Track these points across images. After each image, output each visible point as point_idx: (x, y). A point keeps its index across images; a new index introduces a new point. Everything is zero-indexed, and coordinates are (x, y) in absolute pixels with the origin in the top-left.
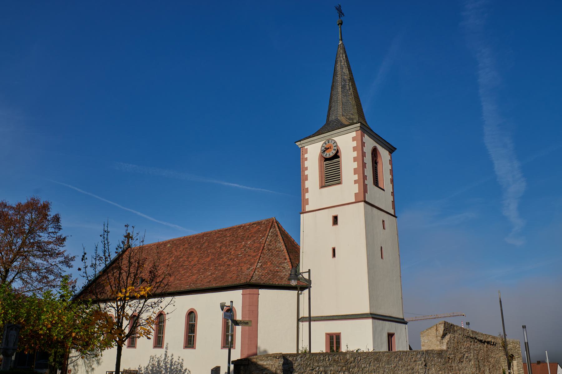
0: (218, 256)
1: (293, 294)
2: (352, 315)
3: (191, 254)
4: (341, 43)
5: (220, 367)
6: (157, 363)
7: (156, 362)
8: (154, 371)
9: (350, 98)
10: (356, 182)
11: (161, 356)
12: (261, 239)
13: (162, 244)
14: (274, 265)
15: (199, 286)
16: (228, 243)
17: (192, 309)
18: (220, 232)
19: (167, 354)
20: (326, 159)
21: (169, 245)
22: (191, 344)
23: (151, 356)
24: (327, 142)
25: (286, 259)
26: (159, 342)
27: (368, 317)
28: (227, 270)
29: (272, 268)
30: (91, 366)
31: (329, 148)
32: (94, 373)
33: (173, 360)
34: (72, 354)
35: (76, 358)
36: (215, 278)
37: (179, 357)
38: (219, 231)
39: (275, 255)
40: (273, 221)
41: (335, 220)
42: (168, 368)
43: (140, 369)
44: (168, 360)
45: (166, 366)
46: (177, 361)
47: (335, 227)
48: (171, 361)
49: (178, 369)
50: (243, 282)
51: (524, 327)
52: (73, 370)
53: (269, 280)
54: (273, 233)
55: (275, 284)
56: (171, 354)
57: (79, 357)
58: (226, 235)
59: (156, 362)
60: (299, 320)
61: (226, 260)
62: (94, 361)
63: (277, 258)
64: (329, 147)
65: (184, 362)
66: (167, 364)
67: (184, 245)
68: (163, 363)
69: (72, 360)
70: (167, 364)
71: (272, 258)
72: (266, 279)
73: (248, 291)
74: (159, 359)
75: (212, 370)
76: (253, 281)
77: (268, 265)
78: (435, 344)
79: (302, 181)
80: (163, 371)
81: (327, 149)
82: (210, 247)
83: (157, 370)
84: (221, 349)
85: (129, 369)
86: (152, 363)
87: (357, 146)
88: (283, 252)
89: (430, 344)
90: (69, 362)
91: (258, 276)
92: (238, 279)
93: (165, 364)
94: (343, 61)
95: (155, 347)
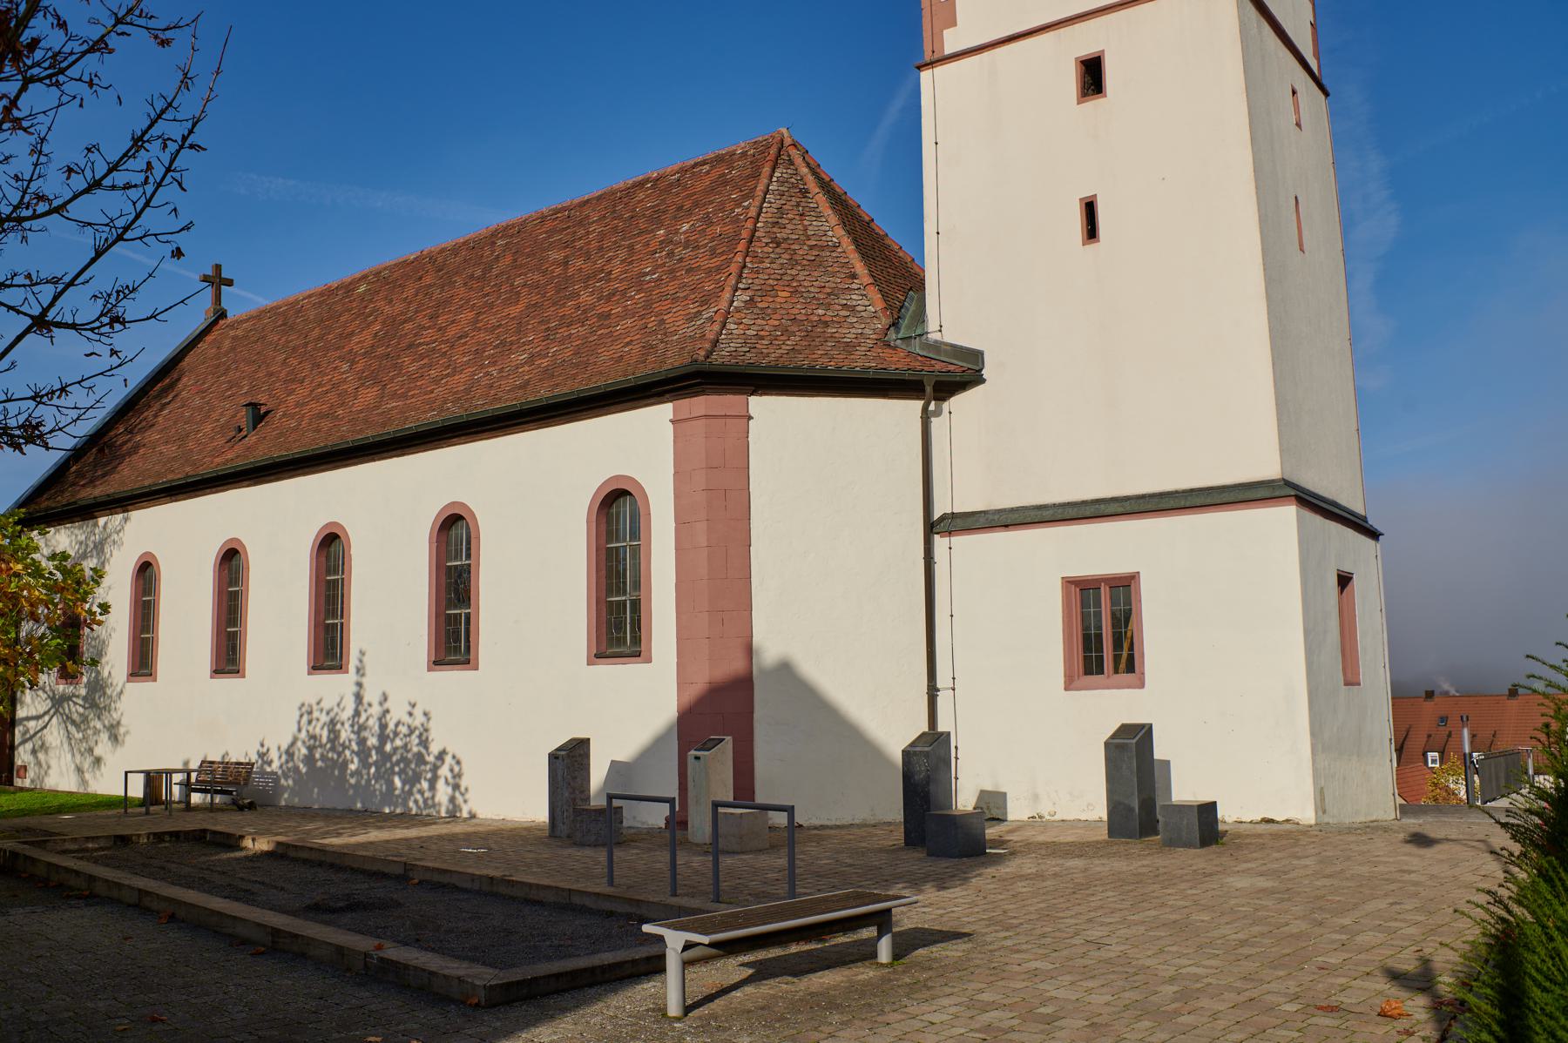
0: (558, 292)
2: (1192, 490)
3: (448, 302)
5: (589, 739)
6: (326, 729)
7: (322, 728)
8: (317, 761)
11: (338, 705)
12: (739, 205)
13: (337, 288)
14: (805, 298)
15: (481, 405)
16: (594, 244)
17: (454, 504)
18: (559, 215)
19: (362, 692)
21: (362, 289)
22: (457, 650)
23: (303, 705)
25: (854, 276)
26: (332, 649)
27: (1277, 494)
28: (600, 332)
29: (798, 310)
30: (91, 750)
32: (102, 775)
33: (388, 717)
34: (25, 709)
35: (41, 723)
36: (546, 370)
37: (414, 706)
38: (557, 211)
39: (805, 262)
40: (782, 141)
41: (1092, 75)
42: (369, 750)
43: (264, 754)
44: (367, 719)
45: (362, 742)
46: (406, 719)
47: (1094, 104)
48: (380, 719)
49: (408, 751)
50: (676, 364)
52: (32, 765)
54: (786, 184)
55: (825, 369)
56: (381, 693)
57: (50, 720)
58: (587, 217)
59: (322, 728)
60: (932, 527)
61: (591, 300)
62: (99, 731)
63: (816, 274)
65: (432, 725)
66: (365, 734)
67: (420, 278)
68: (349, 729)
69: (27, 731)
70: (365, 734)
71: (794, 272)
73: (700, 404)
74: (332, 714)
75: (553, 757)
76: (722, 357)
77: (778, 300)
80: (352, 762)
82: (521, 266)
83: (328, 759)
84: (589, 663)
85: (223, 757)
86: (308, 731)
88: (839, 250)
90: (18, 739)
91: (739, 341)
92: (651, 358)
93: (358, 733)
95: (316, 667)
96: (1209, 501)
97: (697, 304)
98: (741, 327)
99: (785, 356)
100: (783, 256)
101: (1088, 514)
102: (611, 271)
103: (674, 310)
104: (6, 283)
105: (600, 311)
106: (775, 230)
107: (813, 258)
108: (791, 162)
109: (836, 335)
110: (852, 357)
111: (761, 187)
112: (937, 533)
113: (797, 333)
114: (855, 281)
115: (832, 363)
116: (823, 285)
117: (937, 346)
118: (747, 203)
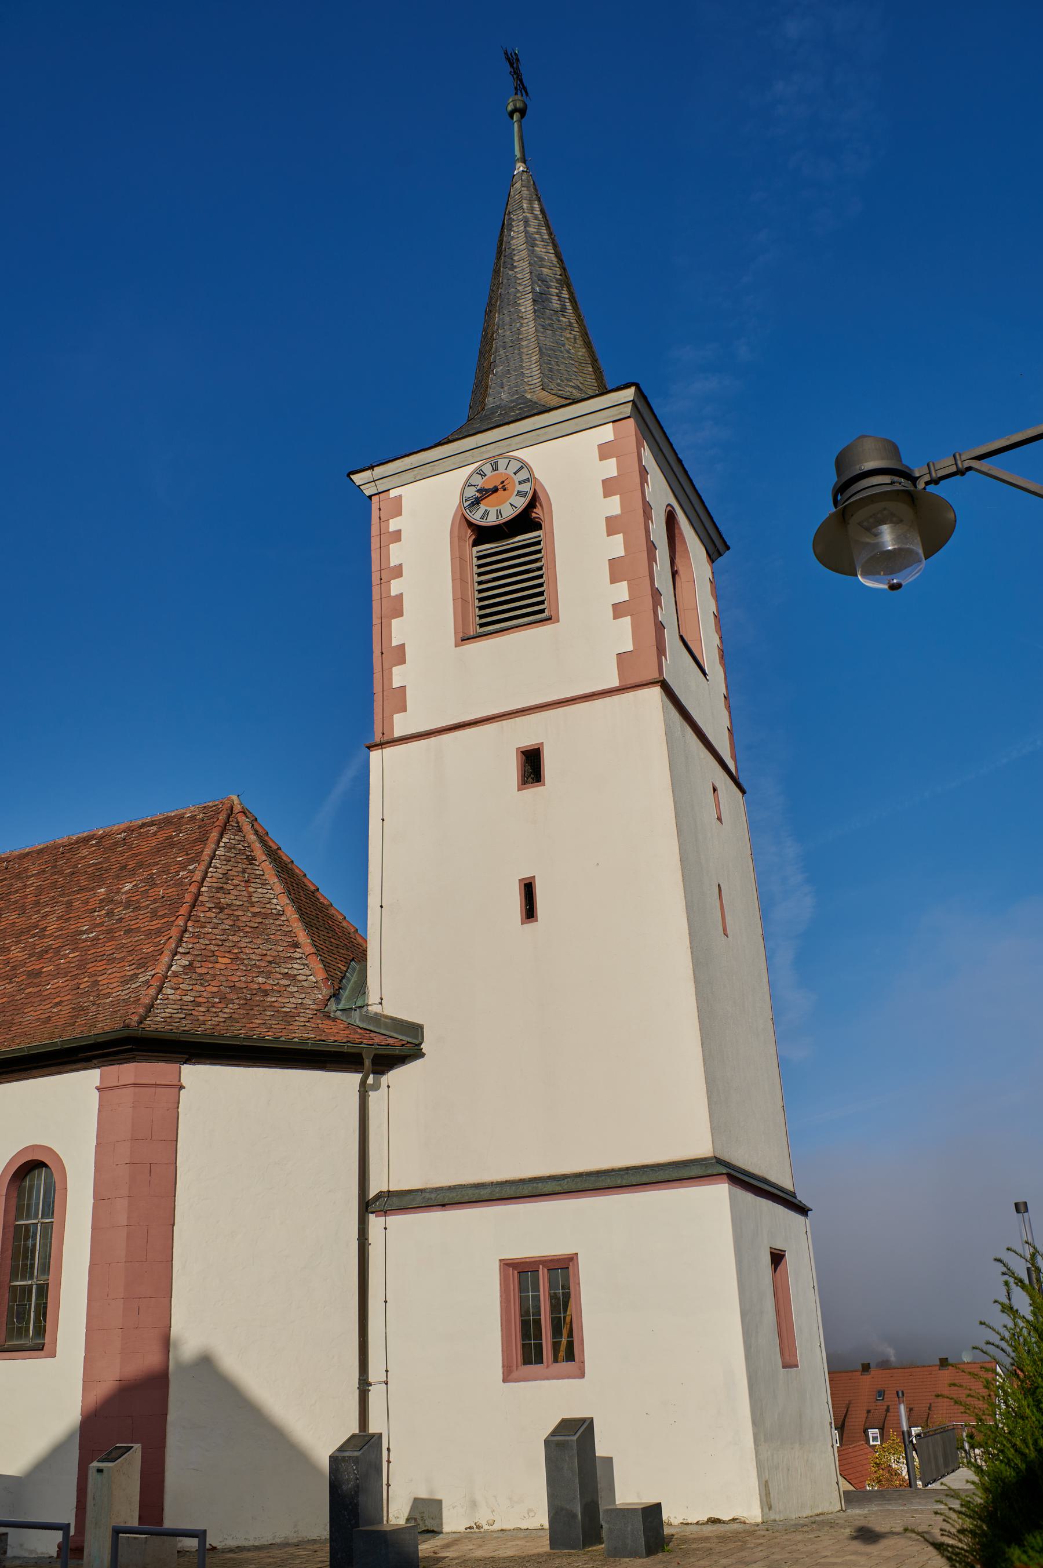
1: (350, 1081)
2: (628, 1169)
4: (521, 169)
9: (568, 339)
10: (618, 610)
12: (184, 868)
14: (246, 966)
16: (31, 898)
20: (483, 534)
24: (487, 469)
25: (296, 945)
27: (709, 1172)
29: (239, 978)
31: (495, 490)
39: (248, 929)
47: (533, 792)
51: (1022, 1209)
53: (229, 1023)
55: (263, 1039)
58: (26, 870)
60: (367, 1206)
63: (258, 941)
64: (497, 483)
71: (236, 938)
72: (216, 1019)
73: (128, 1072)
76: (156, 1023)
77: (218, 966)
79: (376, 620)
81: (486, 493)
87: (618, 475)
91: (175, 1006)
92: (81, 1021)
94: (533, 222)
97: (133, 967)
98: (178, 992)
99: (222, 1024)
100: (225, 921)
101: (526, 1193)
102: (46, 927)
103: (109, 972)
105: (32, 967)
106: (219, 895)
107: (256, 925)
108: (239, 829)
109: (276, 1004)
110: (290, 1027)
111: (208, 852)
112: (373, 1213)
113: (235, 1001)
114: (298, 950)
115: (270, 1033)
116: (265, 952)
117: (377, 1019)
118: (193, 867)
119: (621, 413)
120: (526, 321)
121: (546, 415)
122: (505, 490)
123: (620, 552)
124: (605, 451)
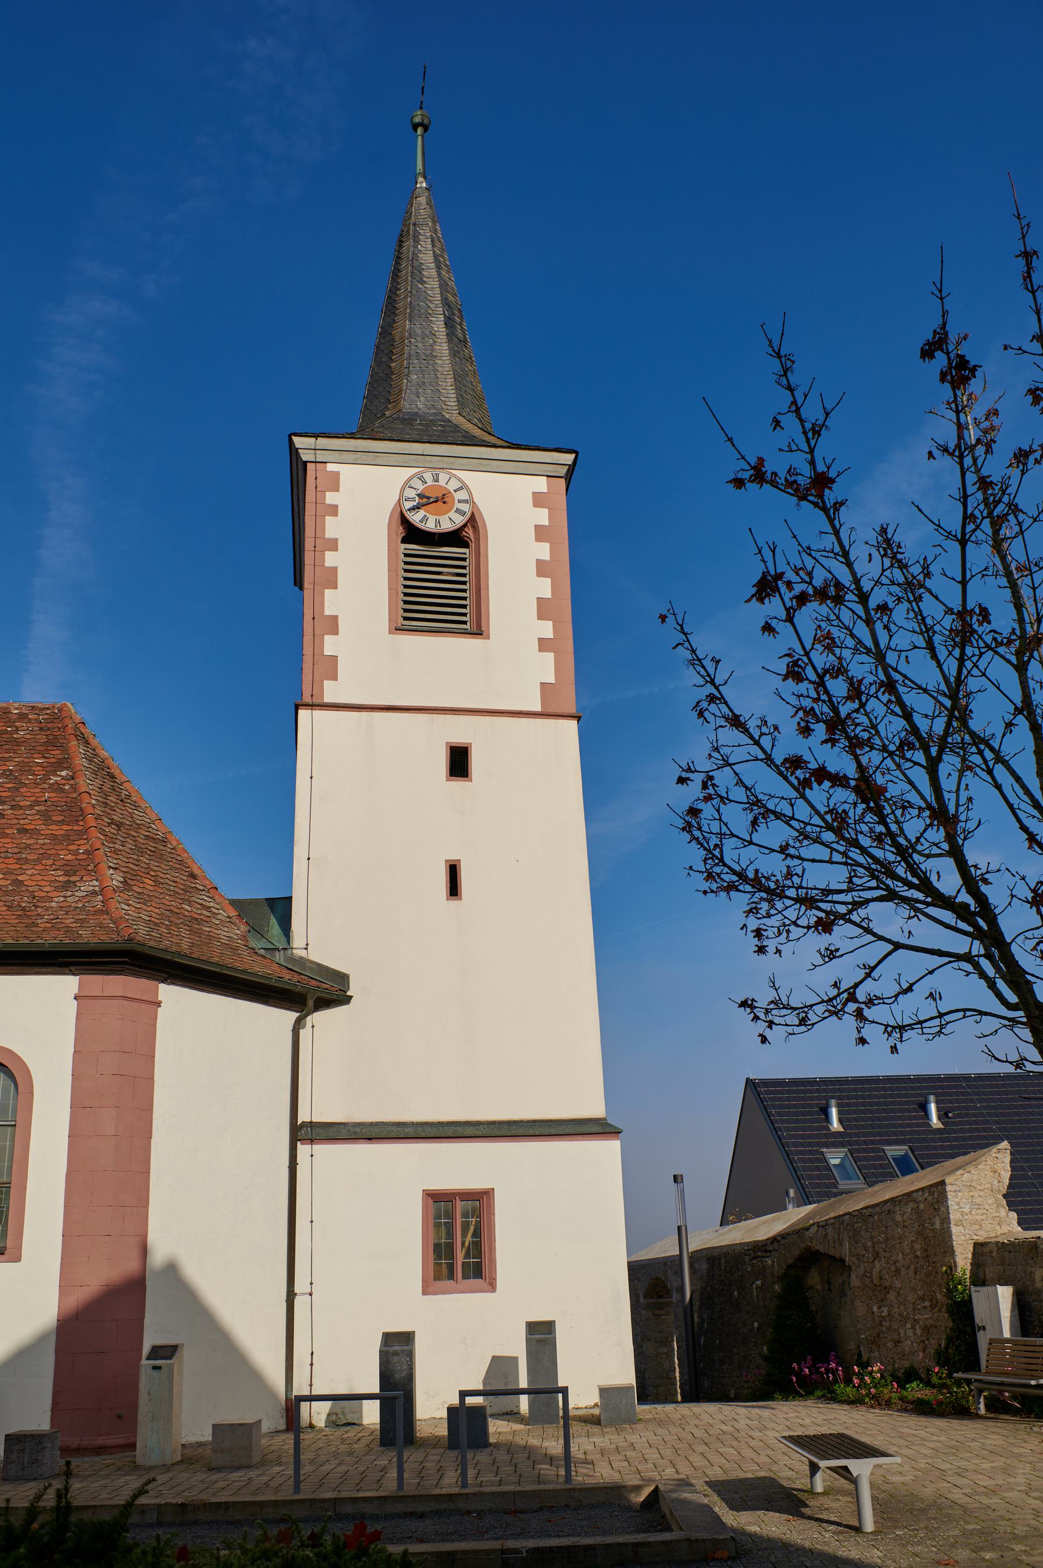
2: (535, 1121)
10: (544, 645)
20: (412, 534)
78: (994, 1217)
89: (979, 1218)
96: (553, 1132)
101: (449, 1134)
104: (900, 713)
112: (299, 1140)
117: (303, 962)
119: (556, 472)
120: (439, 340)
121: (493, 449)
122: (444, 503)
123: (548, 595)
124: (539, 500)
